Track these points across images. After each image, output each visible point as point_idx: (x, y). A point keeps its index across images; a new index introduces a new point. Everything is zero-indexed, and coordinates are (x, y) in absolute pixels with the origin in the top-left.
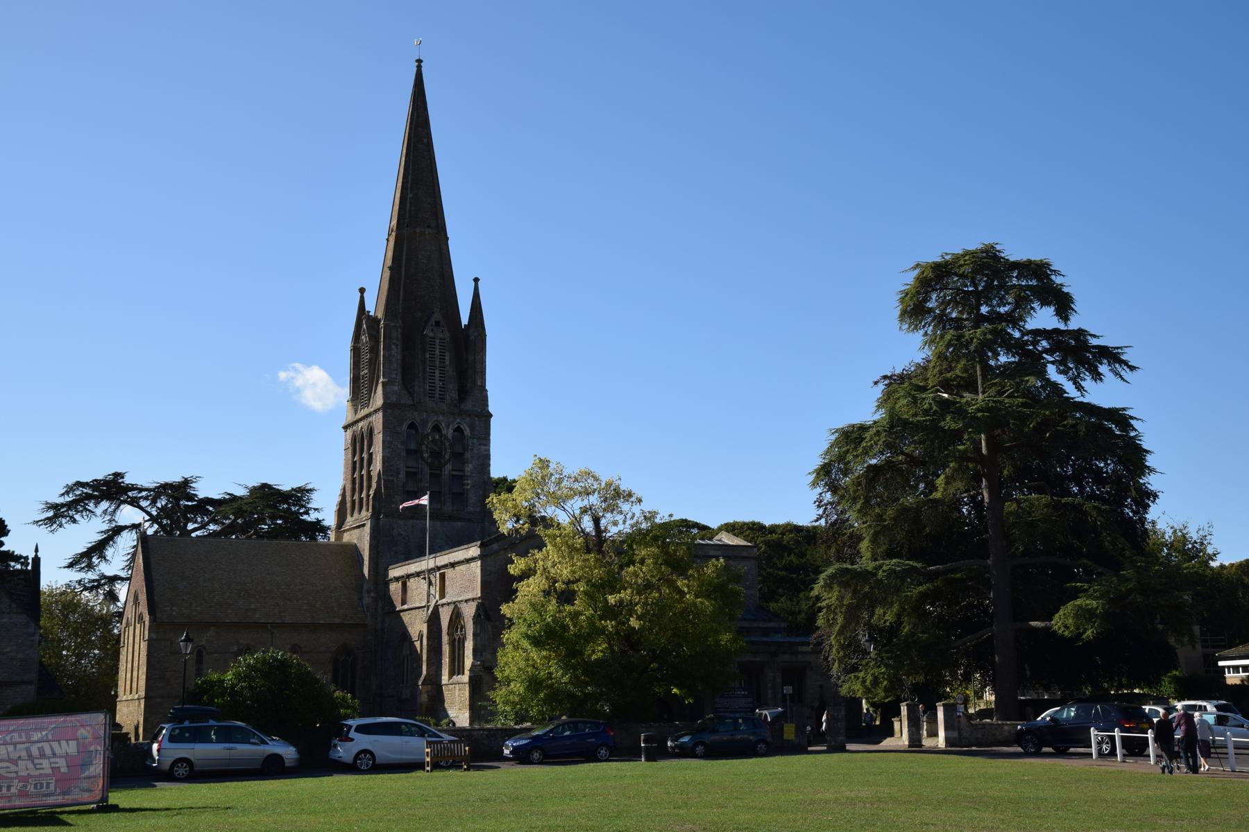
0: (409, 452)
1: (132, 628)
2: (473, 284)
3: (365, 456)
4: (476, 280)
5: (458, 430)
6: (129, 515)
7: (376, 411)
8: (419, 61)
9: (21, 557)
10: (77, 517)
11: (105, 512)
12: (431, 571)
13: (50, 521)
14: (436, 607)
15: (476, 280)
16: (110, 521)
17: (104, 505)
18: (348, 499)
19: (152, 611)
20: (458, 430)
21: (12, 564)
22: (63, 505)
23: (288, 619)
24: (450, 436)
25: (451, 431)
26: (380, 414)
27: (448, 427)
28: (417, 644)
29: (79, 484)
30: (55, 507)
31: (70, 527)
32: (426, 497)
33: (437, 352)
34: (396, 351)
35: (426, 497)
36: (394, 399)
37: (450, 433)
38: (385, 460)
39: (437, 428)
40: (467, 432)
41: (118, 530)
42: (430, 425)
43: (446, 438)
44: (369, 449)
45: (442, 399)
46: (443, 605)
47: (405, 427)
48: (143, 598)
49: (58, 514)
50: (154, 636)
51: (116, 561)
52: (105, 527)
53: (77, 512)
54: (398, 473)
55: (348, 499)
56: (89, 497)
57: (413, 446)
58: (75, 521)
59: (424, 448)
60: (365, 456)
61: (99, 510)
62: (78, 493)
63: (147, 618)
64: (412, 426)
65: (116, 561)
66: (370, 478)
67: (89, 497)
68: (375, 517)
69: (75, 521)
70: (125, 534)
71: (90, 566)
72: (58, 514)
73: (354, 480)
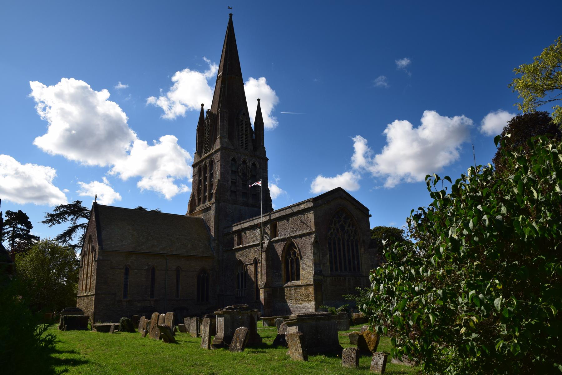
0: (232, 171)
1: (87, 258)
2: (257, 102)
3: (208, 175)
4: (259, 100)
5: (254, 164)
6: (83, 221)
7: (216, 151)
8: (231, 15)
9: (37, 237)
10: (60, 221)
11: (72, 219)
12: (265, 224)
13: (50, 221)
14: (271, 244)
15: (259, 100)
16: (74, 223)
17: (72, 216)
18: (196, 198)
19: (100, 244)
20: (254, 164)
21: (33, 240)
22: (54, 215)
23: (174, 252)
24: (250, 166)
25: (251, 164)
26: (219, 153)
27: (249, 162)
28: (251, 269)
29: (62, 206)
30: (51, 215)
31: (57, 225)
32: (260, 182)
33: (244, 127)
34: (226, 123)
35: (260, 182)
36: (225, 145)
37: (250, 165)
38: (222, 174)
39: (244, 162)
40: (258, 166)
41: (77, 227)
42: (242, 160)
43: (249, 167)
44: (211, 170)
45: (246, 149)
46: (277, 241)
47: (230, 159)
48: (95, 237)
49: (53, 219)
50: (101, 258)
51: (76, 238)
52: (72, 225)
53: (61, 219)
54: (228, 181)
55: (196, 198)
56: (66, 213)
57: (234, 169)
58: (59, 223)
59: (239, 170)
60: (208, 175)
61: (70, 218)
62: (61, 210)
63: (97, 248)
64: (234, 160)
65: (76, 238)
66: (211, 185)
67: (66, 213)
68: (218, 201)
69: (59, 223)
70: (80, 228)
71: (65, 241)
72: (53, 219)
73: (199, 190)
